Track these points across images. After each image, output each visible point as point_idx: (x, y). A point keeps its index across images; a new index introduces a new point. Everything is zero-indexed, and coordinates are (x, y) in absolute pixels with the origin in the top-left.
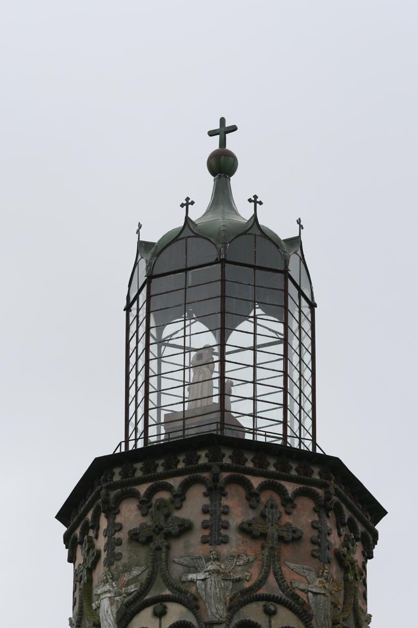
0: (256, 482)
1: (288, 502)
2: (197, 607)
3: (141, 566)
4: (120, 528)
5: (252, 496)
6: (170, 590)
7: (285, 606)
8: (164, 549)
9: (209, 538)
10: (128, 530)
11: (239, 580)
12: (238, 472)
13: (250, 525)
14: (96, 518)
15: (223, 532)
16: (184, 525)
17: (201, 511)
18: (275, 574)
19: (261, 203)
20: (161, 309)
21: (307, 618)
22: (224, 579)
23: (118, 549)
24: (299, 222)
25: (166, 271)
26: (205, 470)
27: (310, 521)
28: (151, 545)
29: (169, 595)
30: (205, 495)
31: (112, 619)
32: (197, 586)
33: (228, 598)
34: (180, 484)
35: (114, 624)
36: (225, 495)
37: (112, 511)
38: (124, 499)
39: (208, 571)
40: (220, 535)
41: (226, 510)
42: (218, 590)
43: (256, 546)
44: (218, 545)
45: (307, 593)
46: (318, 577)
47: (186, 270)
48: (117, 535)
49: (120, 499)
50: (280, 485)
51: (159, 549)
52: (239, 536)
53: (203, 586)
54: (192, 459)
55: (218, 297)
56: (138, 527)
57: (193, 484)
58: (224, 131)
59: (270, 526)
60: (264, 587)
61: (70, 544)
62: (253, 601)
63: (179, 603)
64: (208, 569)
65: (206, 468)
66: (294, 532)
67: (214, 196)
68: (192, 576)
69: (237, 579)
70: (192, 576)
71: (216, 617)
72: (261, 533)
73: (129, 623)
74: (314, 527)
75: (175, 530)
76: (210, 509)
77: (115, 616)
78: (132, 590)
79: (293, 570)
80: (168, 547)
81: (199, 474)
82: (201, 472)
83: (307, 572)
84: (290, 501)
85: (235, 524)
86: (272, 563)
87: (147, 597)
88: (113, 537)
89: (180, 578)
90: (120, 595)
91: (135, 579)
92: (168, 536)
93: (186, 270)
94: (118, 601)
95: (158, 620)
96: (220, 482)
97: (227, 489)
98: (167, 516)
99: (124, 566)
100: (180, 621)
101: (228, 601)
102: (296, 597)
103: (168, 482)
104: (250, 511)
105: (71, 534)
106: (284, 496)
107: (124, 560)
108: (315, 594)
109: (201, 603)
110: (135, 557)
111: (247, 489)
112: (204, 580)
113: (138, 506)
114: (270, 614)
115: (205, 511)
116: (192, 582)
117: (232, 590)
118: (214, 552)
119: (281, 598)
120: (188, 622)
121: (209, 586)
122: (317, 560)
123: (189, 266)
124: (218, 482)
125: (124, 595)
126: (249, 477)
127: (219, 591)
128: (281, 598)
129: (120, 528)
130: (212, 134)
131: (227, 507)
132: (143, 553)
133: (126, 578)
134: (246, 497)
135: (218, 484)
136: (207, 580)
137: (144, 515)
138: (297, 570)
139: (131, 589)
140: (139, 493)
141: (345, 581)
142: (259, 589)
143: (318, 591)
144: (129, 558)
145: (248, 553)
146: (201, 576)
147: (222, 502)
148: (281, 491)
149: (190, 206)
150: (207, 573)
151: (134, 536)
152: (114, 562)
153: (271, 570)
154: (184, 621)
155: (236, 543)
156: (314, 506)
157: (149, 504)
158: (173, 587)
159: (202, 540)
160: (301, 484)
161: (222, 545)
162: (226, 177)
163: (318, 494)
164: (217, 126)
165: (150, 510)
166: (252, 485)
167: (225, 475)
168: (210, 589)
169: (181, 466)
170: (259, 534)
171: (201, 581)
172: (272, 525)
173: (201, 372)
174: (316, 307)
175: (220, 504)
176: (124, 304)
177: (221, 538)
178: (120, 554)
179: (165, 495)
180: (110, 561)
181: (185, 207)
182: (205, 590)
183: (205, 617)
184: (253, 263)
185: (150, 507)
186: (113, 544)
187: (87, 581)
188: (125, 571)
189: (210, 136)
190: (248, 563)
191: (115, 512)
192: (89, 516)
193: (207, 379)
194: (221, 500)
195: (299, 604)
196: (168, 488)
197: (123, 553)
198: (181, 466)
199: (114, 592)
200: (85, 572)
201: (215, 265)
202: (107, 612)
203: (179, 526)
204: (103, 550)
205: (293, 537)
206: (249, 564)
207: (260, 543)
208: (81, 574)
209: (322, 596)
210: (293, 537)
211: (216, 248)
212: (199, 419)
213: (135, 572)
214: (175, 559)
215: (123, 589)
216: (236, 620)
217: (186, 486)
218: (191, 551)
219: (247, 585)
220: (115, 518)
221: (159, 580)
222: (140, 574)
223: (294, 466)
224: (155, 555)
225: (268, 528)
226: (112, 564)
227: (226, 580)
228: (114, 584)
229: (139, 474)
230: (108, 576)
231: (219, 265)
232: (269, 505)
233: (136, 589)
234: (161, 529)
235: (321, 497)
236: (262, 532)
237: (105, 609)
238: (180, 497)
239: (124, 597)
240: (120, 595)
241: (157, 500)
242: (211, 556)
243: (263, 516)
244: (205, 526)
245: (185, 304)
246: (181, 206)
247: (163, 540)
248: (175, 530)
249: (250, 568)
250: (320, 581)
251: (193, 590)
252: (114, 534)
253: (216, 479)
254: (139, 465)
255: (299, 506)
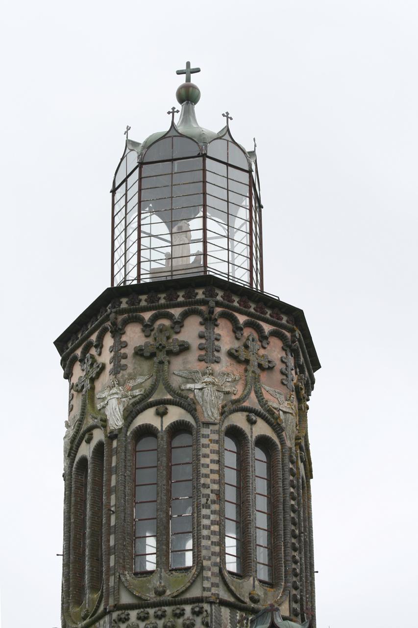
0: (242, 319)
1: (263, 338)
2: (195, 410)
3: (145, 375)
4: (125, 345)
5: (237, 329)
6: (170, 395)
7: (262, 419)
8: (166, 363)
9: (205, 357)
10: (133, 347)
11: (228, 393)
12: (228, 309)
13: (237, 351)
14: (101, 338)
15: (216, 354)
16: (183, 345)
17: (198, 336)
18: (256, 392)
19: (231, 119)
20: (151, 188)
21: (280, 430)
22: (217, 390)
23: (123, 362)
24: (58, 555)
25: (155, 160)
26: (202, 304)
27: (280, 356)
28: (155, 359)
29: (170, 399)
30: (201, 324)
31: (120, 415)
32: (195, 394)
33: (220, 406)
34: (181, 313)
35: (121, 419)
36: (217, 326)
37: (117, 332)
38: (129, 323)
39: (205, 382)
40: (213, 355)
41: (218, 337)
42: (213, 398)
43: (241, 368)
44: (212, 363)
45: (279, 411)
46: (286, 400)
47: (173, 160)
48: (123, 351)
49: (126, 323)
50: (259, 324)
51: (161, 363)
52: (227, 358)
53: (200, 394)
54: (190, 295)
55: (201, 182)
56: (143, 344)
57: (190, 315)
58: (189, 71)
59: (252, 355)
60: (247, 401)
61: (67, 363)
62: (239, 411)
63: (178, 406)
64: (205, 380)
65: (204, 302)
66: (269, 362)
67: (184, 116)
68: (189, 386)
69: (226, 392)
70: (189, 386)
71: (211, 419)
72: (245, 359)
73: (134, 419)
74: (283, 362)
75: (176, 349)
76: (206, 335)
77: (122, 413)
78: (137, 394)
79: (268, 391)
80: (169, 362)
81: (197, 307)
82: (198, 305)
83: (278, 396)
84: (266, 338)
85: (225, 349)
86: (253, 384)
87: (151, 400)
88: (120, 352)
89: (180, 387)
90: (126, 397)
91: (139, 386)
92: (170, 353)
93: (173, 160)
94: (124, 402)
95: (159, 419)
96: (214, 314)
97: (219, 322)
98: (168, 338)
99: (130, 374)
100: (180, 420)
101: (220, 408)
102: (272, 413)
103: (170, 311)
104: (236, 341)
105: (150, 307)
106: (261, 333)
107: (130, 370)
108: (285, 412)
109: (198, 407)
110: (139, 369)
111: (234, 324)
112: (201, 389)
113: (142, 329)
114: (252, 422)
115: (201, 337)
116: (190, 390)
117: (223, 400)
118: (210, 368)
119: (260, 412)
120: (186, 421)
121: (206, 394)
122: (285, 387)
123: (241, 266)
124: (213, 315)
125: (130, 397)
126: (236, 314)
127: (214, 399)
128: (260, 412)
129: (125, 345)
130: (179, 73)
131: (125, 342)
132: (146, 365)
133: (131, 384)
134: (233, 330)
135: (213, 316)
136: (203, 389)
137: (147, 336)
138: (271, 392)
139: (136, 393)
140: (144, 319)
141: (299, 410)
142: (244, 402)
143: (287, 411)
144: (133, 369)
145: (235, 373)
146: (199, 386)
147: (215, 331)
148: (259, 329)
149: (175, 114)
150: (205, 384)
151: (139, 353)
152: (120, 372)
153: (253, 389)
154: (183, 421)
155: (225, 365)
156: (282, 345)
157: (152, 328)
158: (175, 393)
159: (199, 359)
160: (275, 326)
161: (215, 364)
162: (192, 104)
163: (286, 336)
164: (184, 68)
165: (153, 333)
166: (238, 320)
167: (218, 310)
168: (207, 396)
169: (181, 299)
170: (243, 359)
171: (198, 390)
172: (253, 354)
173: (181, 239)
174: (263, 208)
175: (214, 332)
176: (111, 188)
177: (214, 358)
178: (126, 365)
179: (167, 323)
180: (117, 371)
181: (171, 114)
182: (202, 398)
183: (202, 418)
184: (226, 161)
185: (152, 330)
186: (118, 358)
187: (90, 388)
188: (131, 379)
189: (178, 74)
190: (234, 381)
191: (122, 332)
192: (94, 338)
193: (181, 246)
194: (214, 329)
195: (273, 418)
196: (170, 316)
197: (128, 364)
198: (181, 299)
199: (121, 394)
200: (88, 381)
201: (197, 158)
202: (115, 409)
203: (180, 346)
204: (109, 363)
205: (269, 366)
206: (236, 382)
207: (242, 367)
208: (83, 383)
209: (290, 415)
210: (269, 366)
211: (199, 146)
212: (183, 272)
213: (140, 380)
214: (175, 372)
215: (129, 392)
216: (226, 424)
217: (185, 315)
218: (189, 366)
219: (234, 397)
220: (121, 338)
221: (161, 386)
222: (144, 382)
223: (269, 312)
224: (158, 367)
225: (250, 356)
226: (119, 373)
227: (219, 391)
228: (120, 388)
229: (143, 303)
230: (115, 382)
231: (201, 159)
232: (251, 338)
233: (140, 393)
234: (164, 347)
235: (288, 339)
236: (246, 358)
237: (114, 406)
238: (178, 325)
239: (130, 399)
240: (127, 397)
241: (160, 325)
242: (208, 371)
243: (246, 347)
244: (201, 348)
245: (172, 185)
246: (168, 113)
247: (165, 356)
248: (176, 349)
249: (237, 385)
250: (288, 404)
251: (191, 396)
252: (120, 350)
253: (211, 312)
254: (144, 297)
255: (271, 344)
